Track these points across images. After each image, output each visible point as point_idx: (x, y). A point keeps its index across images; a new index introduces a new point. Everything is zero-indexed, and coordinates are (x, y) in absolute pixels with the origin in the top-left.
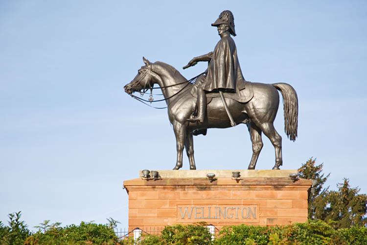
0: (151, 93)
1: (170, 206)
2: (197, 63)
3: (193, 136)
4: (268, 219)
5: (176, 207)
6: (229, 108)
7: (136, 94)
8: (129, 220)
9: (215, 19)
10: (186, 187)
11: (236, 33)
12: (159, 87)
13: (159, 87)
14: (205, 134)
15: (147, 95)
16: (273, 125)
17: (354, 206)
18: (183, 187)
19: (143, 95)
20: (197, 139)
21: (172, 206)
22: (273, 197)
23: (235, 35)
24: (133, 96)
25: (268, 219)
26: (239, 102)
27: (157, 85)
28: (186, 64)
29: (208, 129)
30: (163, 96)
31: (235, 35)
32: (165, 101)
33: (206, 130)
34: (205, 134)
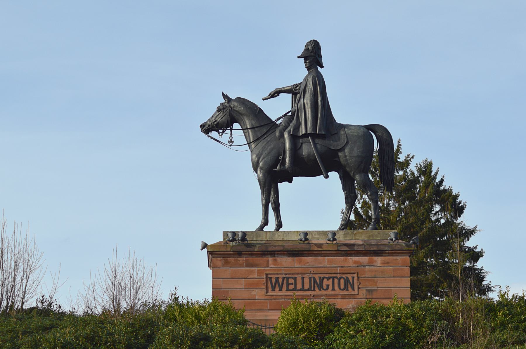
0: (231, 134)
1: (258, 275)
2: (278, 95)
3: (279, 184)
4: (367, 290)
5: (265, 276)
6: (320, 155)
7: (214, 134)
8: (213, 291)
9: (301, 50)
10: (276, 252)
11: (324, 65)
12: (241, 128)
13: (241, 128)
14: (290, 182)
15: (225, 137)
16: (318, 70)
17: (478, 309)
18: (273, 254)
19: (221, 135)
20: (283, 187)
21: (260, 276)
22: (371, 264)
23: (322, 67)
24: (209, 136)
25: (367, 290)
26: (331, 149)
27: (238, 124)
28: (266, 95)
29: (294, 178)
30: (244, 136)
31: (322, 67)
32: (247, 145)
33: (292, 178)
34: (290, 182)
